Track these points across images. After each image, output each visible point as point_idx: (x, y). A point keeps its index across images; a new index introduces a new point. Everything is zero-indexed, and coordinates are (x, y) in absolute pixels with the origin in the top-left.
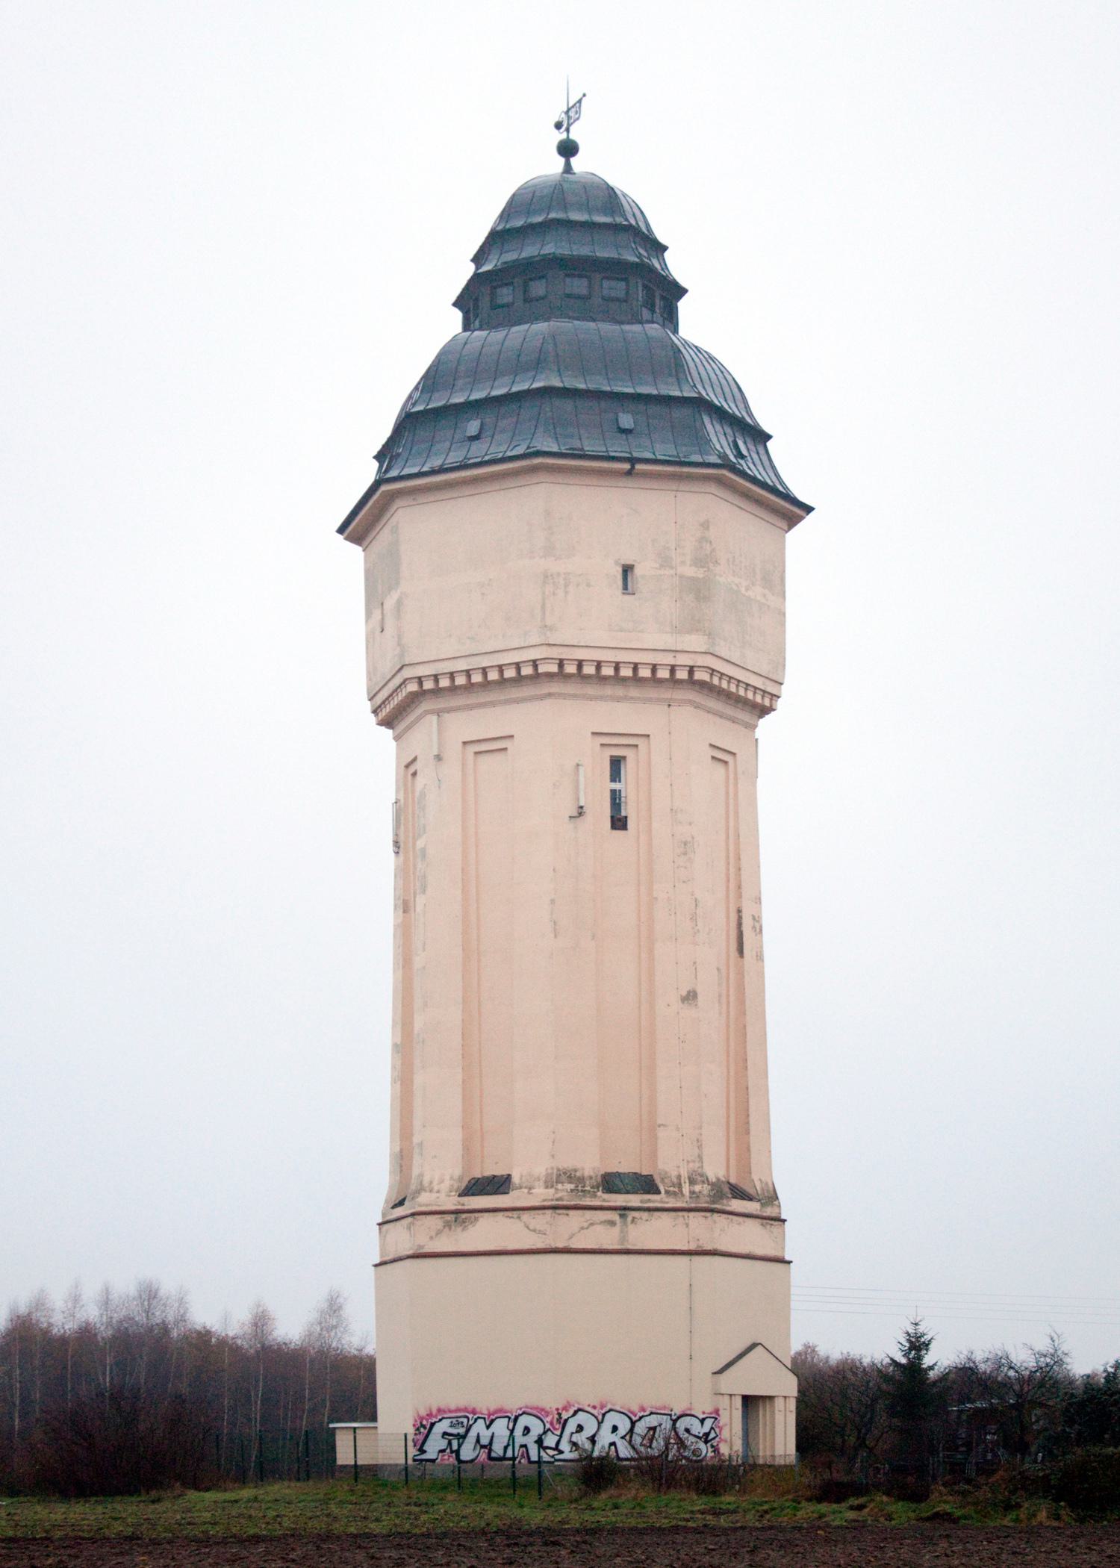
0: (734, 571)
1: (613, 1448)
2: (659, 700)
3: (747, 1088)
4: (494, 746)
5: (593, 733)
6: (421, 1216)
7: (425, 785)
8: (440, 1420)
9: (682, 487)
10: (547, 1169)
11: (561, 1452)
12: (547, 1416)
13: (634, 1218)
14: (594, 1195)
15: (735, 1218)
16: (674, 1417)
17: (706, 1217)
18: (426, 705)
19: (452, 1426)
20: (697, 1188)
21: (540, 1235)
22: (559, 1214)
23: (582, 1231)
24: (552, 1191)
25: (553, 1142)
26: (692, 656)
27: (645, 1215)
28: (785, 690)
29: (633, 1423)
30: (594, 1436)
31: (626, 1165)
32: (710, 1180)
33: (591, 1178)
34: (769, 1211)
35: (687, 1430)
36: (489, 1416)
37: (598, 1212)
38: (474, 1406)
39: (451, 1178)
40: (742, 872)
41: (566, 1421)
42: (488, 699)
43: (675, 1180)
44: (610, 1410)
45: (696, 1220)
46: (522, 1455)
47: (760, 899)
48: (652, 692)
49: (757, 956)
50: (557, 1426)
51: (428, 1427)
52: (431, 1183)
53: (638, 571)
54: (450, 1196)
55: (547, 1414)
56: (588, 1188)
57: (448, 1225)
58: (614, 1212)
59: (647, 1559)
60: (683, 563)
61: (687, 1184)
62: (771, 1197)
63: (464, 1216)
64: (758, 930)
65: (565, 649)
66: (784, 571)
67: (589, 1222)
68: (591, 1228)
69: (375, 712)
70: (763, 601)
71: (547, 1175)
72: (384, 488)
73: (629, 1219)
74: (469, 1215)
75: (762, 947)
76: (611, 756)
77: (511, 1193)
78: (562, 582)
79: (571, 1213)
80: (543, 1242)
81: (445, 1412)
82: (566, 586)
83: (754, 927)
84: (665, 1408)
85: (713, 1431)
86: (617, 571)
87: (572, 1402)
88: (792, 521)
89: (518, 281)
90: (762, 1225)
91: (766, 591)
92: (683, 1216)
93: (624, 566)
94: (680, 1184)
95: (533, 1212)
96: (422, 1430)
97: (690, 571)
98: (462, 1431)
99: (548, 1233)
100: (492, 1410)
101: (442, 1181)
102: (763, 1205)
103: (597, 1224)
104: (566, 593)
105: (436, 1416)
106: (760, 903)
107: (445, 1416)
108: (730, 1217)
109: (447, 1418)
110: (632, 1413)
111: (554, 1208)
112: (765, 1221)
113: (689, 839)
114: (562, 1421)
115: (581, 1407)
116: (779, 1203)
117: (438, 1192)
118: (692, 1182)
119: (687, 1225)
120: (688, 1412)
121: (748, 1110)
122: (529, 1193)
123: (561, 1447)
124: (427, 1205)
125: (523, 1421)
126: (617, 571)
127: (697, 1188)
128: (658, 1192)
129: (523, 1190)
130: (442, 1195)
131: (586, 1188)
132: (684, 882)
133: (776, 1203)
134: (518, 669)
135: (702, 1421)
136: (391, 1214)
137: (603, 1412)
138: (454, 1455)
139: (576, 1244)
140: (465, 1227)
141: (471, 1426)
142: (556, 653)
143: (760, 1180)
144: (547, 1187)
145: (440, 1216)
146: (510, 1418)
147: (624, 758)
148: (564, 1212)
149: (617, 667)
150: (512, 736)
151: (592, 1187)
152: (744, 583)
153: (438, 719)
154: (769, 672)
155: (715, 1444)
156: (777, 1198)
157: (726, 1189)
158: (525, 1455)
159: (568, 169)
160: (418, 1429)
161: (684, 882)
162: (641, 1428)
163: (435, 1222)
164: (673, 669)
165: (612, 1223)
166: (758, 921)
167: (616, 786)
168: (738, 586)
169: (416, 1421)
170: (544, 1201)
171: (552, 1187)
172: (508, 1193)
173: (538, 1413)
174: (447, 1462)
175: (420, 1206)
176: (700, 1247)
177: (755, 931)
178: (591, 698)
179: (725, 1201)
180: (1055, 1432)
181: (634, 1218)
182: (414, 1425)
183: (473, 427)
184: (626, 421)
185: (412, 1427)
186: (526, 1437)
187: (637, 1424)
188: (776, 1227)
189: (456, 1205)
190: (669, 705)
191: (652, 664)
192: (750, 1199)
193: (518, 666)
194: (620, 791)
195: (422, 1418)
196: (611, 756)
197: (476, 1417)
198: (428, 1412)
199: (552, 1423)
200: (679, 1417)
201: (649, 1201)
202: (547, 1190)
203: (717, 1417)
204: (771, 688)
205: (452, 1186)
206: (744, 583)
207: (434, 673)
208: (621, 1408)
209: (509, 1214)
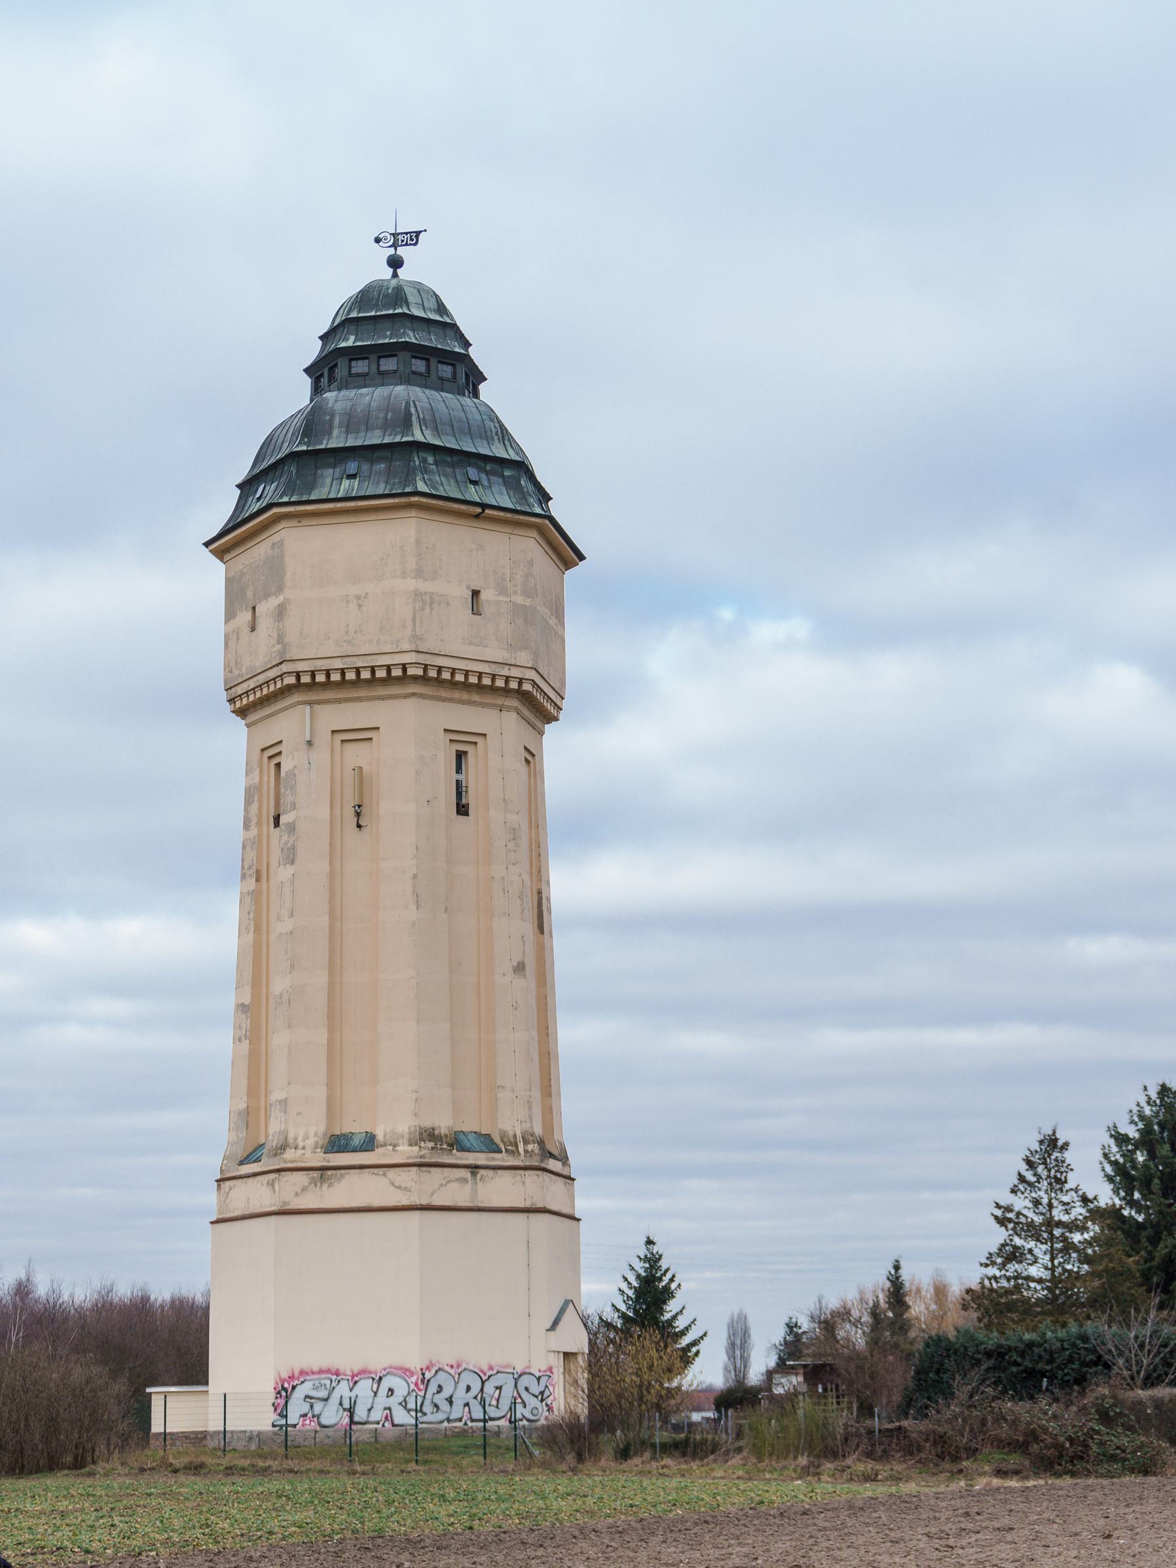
1: (467, 1408)
2: (493, 706)
3: (549, 1054)
4: (362, 735)
5: (445, 730)
6: (287, 1173)
7: (295, 766)
8: (302, 1382)
9: (517, 531)
10: (410, 1127)
11: (425, 1414)
12: (412, 1376)
13: (482, 1176)
17: (538, 1176)
18: (296, 698)
19: (315, 1388)
20: (530, 1147)
22: (423, 1171)
23: (441, 1189)
24: (416, 1148)
25: (416, 1101)
27: (490, 1173)
29: (483, 1383)
30: (451, 1397)
31: (469, 1124)
33: (446, 1136)
35: (527, 1389)
36: (352, 1378)
37: (455, 1170)
38: (338, 1367)
39: (316, 1135)
40: (541, 857)
41: (429, 1380)
42: (356, 695)
43: (512, 1140)
44: (465, 1369)
45: (531, 1177)
46: (386, 1418)
50: (421, 1387)
52: (296, 1139)
53: (483, 596)
54: (315, 1152)
55: (412, 1374)
57: (313, 1182)
58: (466, 1170)
59: (312, 1523)
60: (515, 592)
61: (522, 1144)
63: (330, 1173)
65: (429, 656)
68: (449, 1185)
69: (232, 701)
71: (410, 1133)
72: (275, 510)
73: (479, 1176)
74: (334, 1172)
76: (457, 751)
77: (376, 1150)
78: (428, 600)
79: (433, 1170)
81: (307, 1374)
82: (431, 603)
84: (507, 1366)
85: (547, 1389)
87: (434, 1361)
88: (568, 564)
89: (374, 357)
92: (521, 1175)
94: (517, 1143)
95: (398, 1169)
97: (519, 600)
98: (323, 1394)
100: (355, 1371)
101: (306, 1138)
104: (432, 609)
109: (310, 1380)
110: (482, 1372)
111: (420, 1165)
113: (517, 826)
114: (426, 1381)
115: (441, 1366)
117: (304, 1148)
118: (526, 1142)
119: (524, 1183)
120: (527, 1371)
121: (550, 1074)
122: (393, 1150)
123: (424, 1409)
125: (387, 1383)
127: (530, 1147)
128: (501, 1152)
129: (388, 1147)
130: (308, 1152)
132: (514, 864)
134: (373, 672)
135: (539, 1379)
136: (238, 1170)
137: (459, 1371)
138: (315, 1419)
139: (437, 1201)
141: (334, 1388)
142: (422, 659)
144: (411, 1145)
145: (305, 1172)
146: (373, 1379)
150: (378, 728)
155: (549, 1403)
158: (389, 1418)
159: (395, 275)
160: (279, 1393)
161: (514, 864)
162: (489, 1388)
163: (301, 1178)
165: (465, 1181)
167: (460, 777)
169: (277, 1384)
170: (408, 1158)
171: (416, 1144)
172: (374, 1150)
173: (405, 1372)
174: (307, 1427)
175: (286, 1162)
176: (535, 1204)
178: (444, 700)
180: (72, 1368)
182: (275, 1388)
184: (473, 473)
185: (273, 1391)
186: (391, 1399)
187: (486, 1383)
189: (320, 1161)
190: (501, 710)
191: (387, 665)
193: (389, 668)
195: (283, 1381)
196: (457, 751)
197: (339, 1378)
198: (291, 1375)
199: (416, 1385)
201: (488, 1159)
202: (411, 1148)
203: (550, 1374)
208: (474, 1367)
209: (376, 1171)
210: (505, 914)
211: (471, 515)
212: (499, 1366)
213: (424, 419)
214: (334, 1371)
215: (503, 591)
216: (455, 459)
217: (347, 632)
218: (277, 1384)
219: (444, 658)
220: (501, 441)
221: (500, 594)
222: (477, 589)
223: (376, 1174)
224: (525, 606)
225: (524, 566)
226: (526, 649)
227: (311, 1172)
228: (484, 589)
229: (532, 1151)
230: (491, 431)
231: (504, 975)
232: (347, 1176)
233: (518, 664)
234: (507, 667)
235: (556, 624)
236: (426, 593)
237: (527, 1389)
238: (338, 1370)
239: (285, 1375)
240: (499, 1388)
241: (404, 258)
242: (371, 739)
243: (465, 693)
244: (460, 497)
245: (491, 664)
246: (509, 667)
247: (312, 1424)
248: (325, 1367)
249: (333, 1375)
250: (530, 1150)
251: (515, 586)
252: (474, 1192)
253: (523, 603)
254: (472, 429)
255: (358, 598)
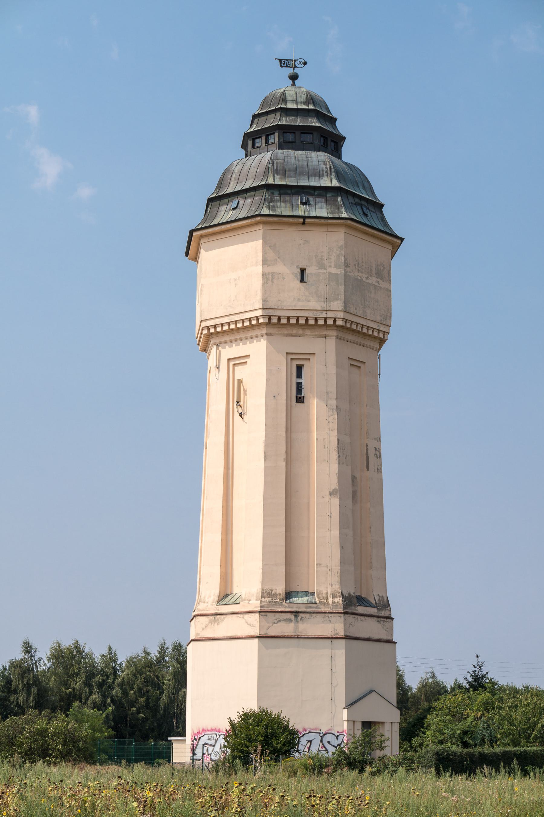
0: (358, 270)
2: (320, 336)
8: (204, 736)
13: (302, 617)
14: (281, 604)
15: (359, 617)
16: (321, 735)
20: (336, 600)
21: (253, 627)
26: (335, 313)
27: (308, 616)
28: (391, 330)
32: (344, 596)
33: (280, 594)
34: (383, 613)
35: (329, 742)
37: (283, 614)
39: (214, 595)
43: (325, 596)
47: (380, 439)
48: (318, 332)
49: (378, 470)
51: (198, 739)
52: (205, 597)
53: (308, 271)
54: (212, 605)
56: (278, 600)
60: (330, 266)
62: (385, 605)
63: (218, 617)
64: (378, 456)
65: (271, 311)
66: (390, 270)
67: (278, 620)
70: (377, 284)
73: (299, 618)
75: (381, 465)
76: (296, 365)
78: (270, 277)
79: (268, 614)
80: (254, 631)
83: (376, 454)
84: (316, 729)
86: (298, 271)
90: (378, 621)
91: (379, 280)
92: (328, 616)
93: (301, 269)
94: (327, 598)
96: (195, 741)
98: (212, 742)
99: (256, 626)
102: (379, 610)
103: (282, 621)
104: (272, 282)
105: (201, 734)
106: (380, 441)
107: (206, 733)
108: (356, 616)
112: (379, 619)
116: (390, 608)
117: (207, 603)
124: (202, 610)
126: (298, 271)
127: (336, 600)
130: (209, 605)
131: (277, 600)
133: (388, 608)
135: (337, 737)
138: (209, 756)
140: (219, 623)
141: (217, 739)
143: (379, 595)
147: (304, 365)
148: (265, 614)
149: (298, 319)
151: (281, 600)
152: (365, 276)
153: (217, 347)
154: (381, 320)
156: (389, 606)
157: (355, 600)
160: (193, 741)
161: (332, 430)
163: (204, 620)
164: (325, 320)
166: (379, 451)
167: (300, 380)
168: (361, 277)
169: (192, 736)
170: (255, 607)
175: (199, 610)
177: (377, 456)
179: (353, 608)
181: (302, 617)
182: (191, 739)
183: (234, 204)
188: (387, 623)
189: (215, 610)
190: (326, 338)
191: (334, 318)
192: (371, 606)
194: (301, 383)
195: (195, 735)
196: (296, 365)
197: (220, 734)
198: (198, 732)
200: (325, 735)
204: (382, 328)
205: (214, 599)
206: (365, 276)
207: (214, 324)
209: (239, 615)
210: (325, 460)
211: (299, 224)
212: (310, 729)
213: (277, 170)
214: (217, 730)
215: (321, 266)
216: (293, 191)
217: (230, 301)
218: (192, 736)
219: (281, 310)
220: (329, 176)
221: (319, 268)
222: (304, 267)
223: (239, 617)
224: (337, 274)
225: (337, 250)
226: (337, 299)
227: (209, 617)
228: (309, 267)
229: (338, 602)
230: (323, 171)
231: (323, 497)
232: (226, 618)
233: (331, 309)
234: (325, 312)
235: (378, 282)
236: (269, 273)
237: (329, 742)
238: (219, 729)
239: (196, 732)
240: (310, 742)
241: (298, 73)
242: (309, 359)
243: (301, 329)
244: (291, 214)
245: (313, 311)
246: (326, 312)
247: (208, 759)
248: (214, 728)
249: (217, 732)
250: (336, 601)
251: (331, 263)
252: (296, 628)
253: (336, 272)
254: (310, 171)
255: (235, 280)
